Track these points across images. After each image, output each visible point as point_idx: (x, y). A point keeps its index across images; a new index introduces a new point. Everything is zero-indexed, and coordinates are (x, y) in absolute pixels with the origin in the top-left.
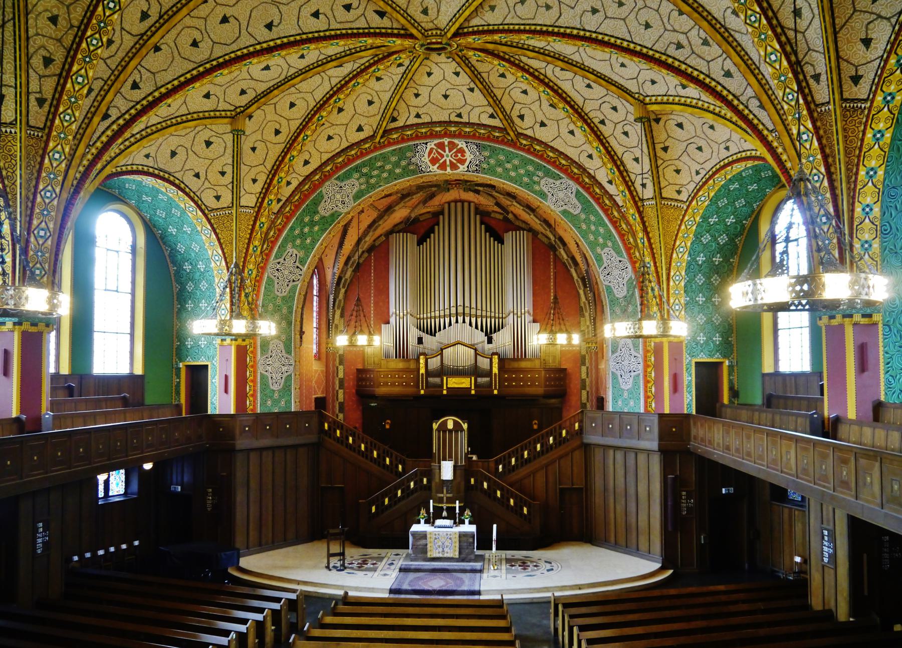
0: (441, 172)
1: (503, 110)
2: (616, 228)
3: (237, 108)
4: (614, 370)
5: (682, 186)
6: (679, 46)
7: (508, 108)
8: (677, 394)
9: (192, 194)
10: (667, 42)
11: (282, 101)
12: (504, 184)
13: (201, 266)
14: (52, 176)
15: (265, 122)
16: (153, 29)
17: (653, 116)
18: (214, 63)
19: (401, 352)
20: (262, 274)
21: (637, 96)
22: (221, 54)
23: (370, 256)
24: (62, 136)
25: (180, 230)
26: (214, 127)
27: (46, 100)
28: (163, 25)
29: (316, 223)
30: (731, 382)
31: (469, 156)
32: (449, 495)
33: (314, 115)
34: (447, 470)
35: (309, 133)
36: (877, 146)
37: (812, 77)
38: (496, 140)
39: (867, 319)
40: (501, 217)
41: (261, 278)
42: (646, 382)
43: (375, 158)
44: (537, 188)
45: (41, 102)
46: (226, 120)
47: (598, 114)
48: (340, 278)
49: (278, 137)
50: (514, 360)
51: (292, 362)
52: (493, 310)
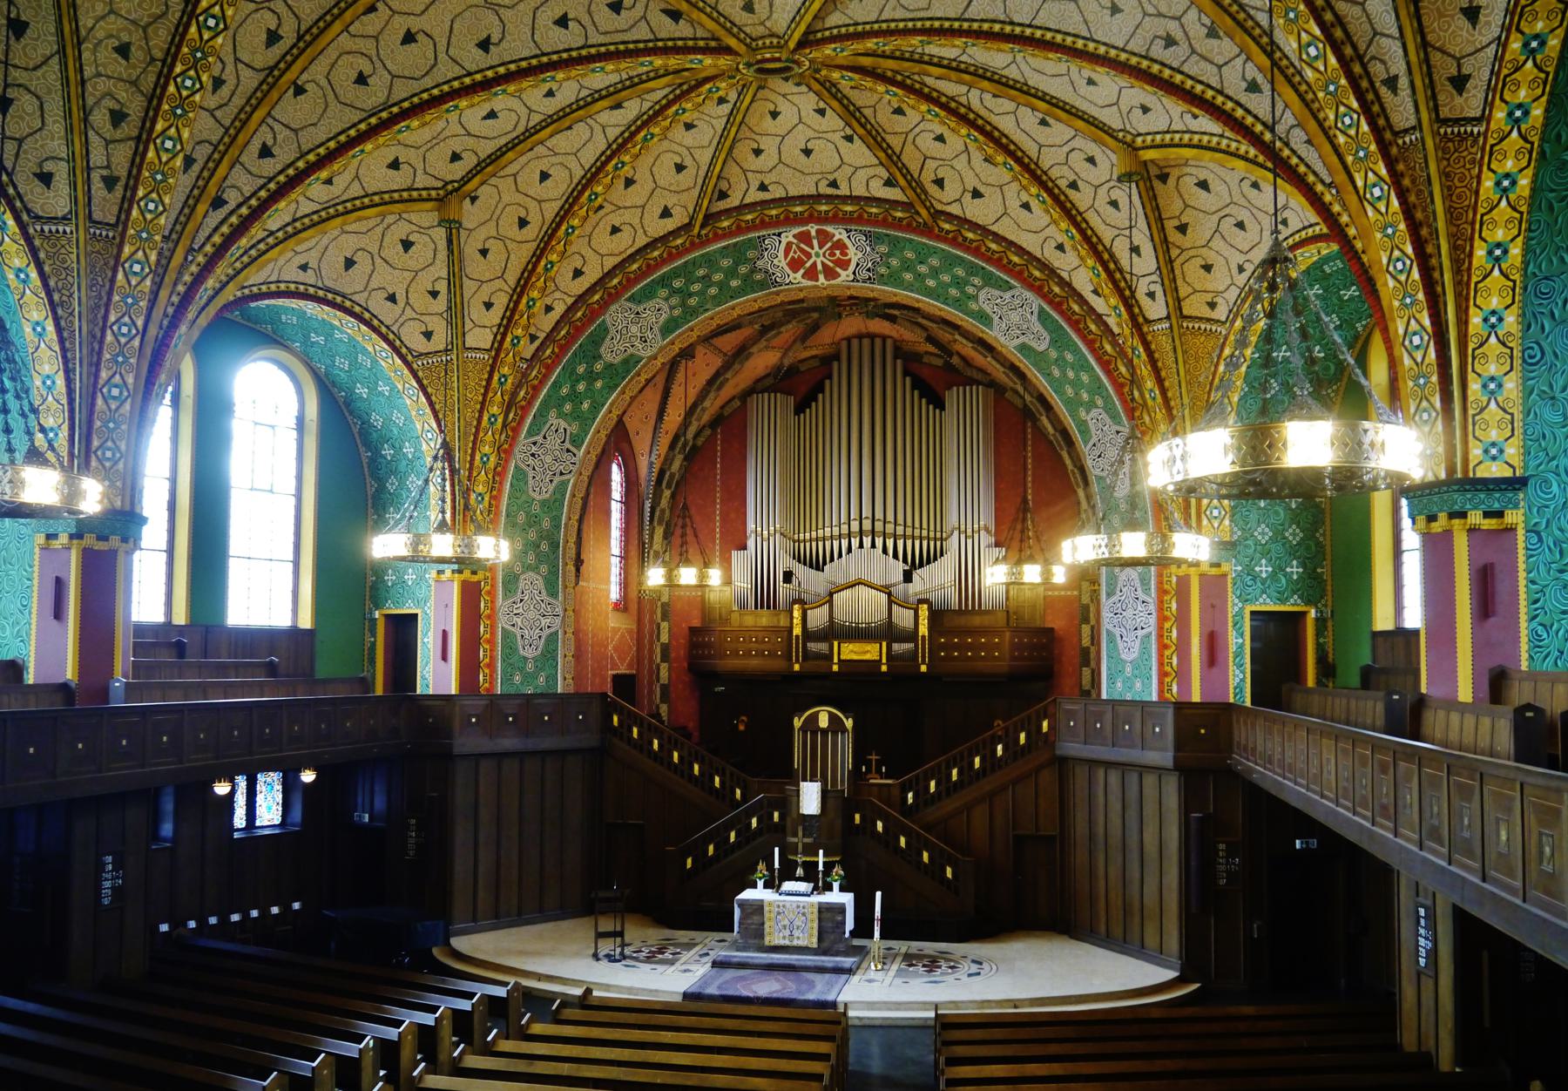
0: (810, 283)
1: (905, 171)
2: (1108, 373)
3: (447, 183)
4: (1110, 627)
5: (1218, 293)
6: (1170, 42)
7: (914, 168)
8: (1215, 670)
9: (384, 330)
10: (1149, 36)
11: (527, 170)
12: (918, 301)
13: (408, 450)
14: (130, 301)
15: (500, 206)
16: (289, 58)
17: (1154, 171)
18: (395, 110)
19: (764, 598)
20: (507, 461)
21: (1121, 135)
22: (405, 95)
23: (714, 434)
24: (144, 235)
25: (372, 389)
26: (413, 217)
27: (117, 179)
28: (304, 50)
29: (598, 376)
30: (1320, 648)
31: (854, 255)
32: (806, 840)
33: (581, 193)
34: (810, 798)
35: (576, 222)
36: (1504, 203)
37: (1384, 82)
38: (897, 224)
39: (1494, 521)
40: (939, 362)
41: (505, 468)
42: (1162, 647)
43: (694, 262)
44: (974, 306)
45: (110, 182)
46: (430, 205)
47: (1065, 170)
48: (662, 473)
49: (525, 230)
50: (960, 612)
51: (559, 610)
52: (925, 525)
